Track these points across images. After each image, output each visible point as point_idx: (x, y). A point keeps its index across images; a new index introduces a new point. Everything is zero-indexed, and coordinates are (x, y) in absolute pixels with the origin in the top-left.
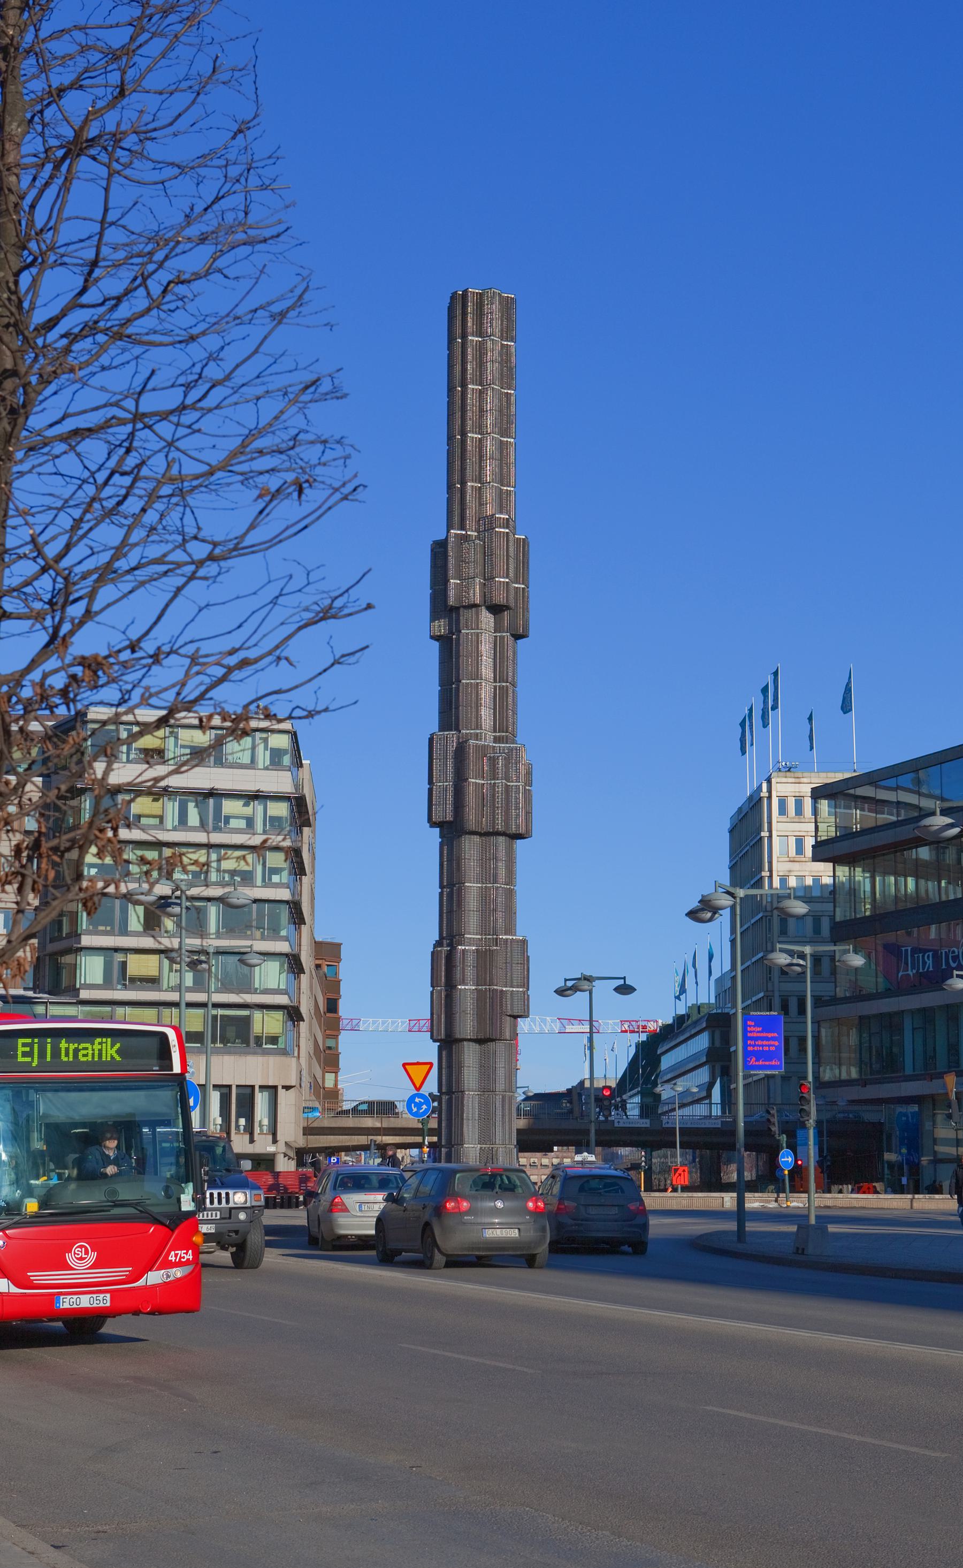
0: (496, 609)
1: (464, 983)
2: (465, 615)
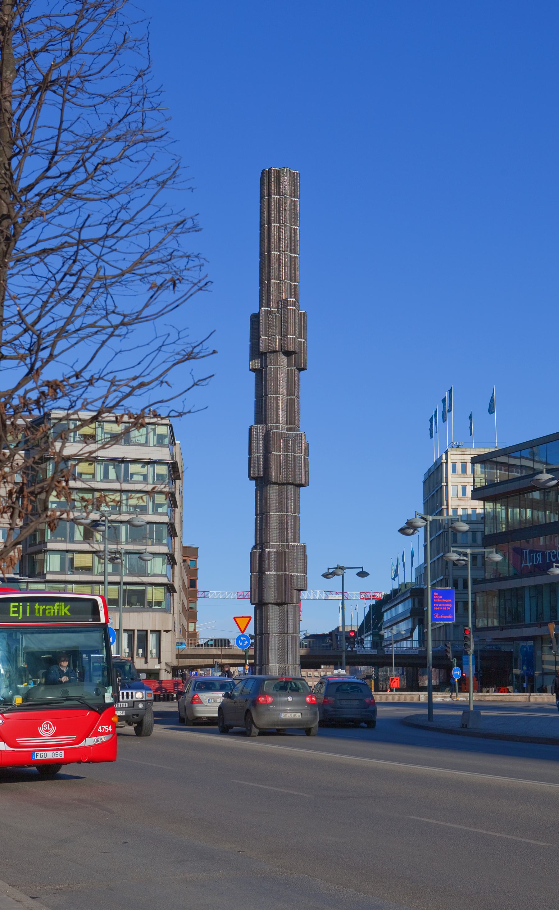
0: (288, 354)
1: (269, 571)
2: (270, 357)
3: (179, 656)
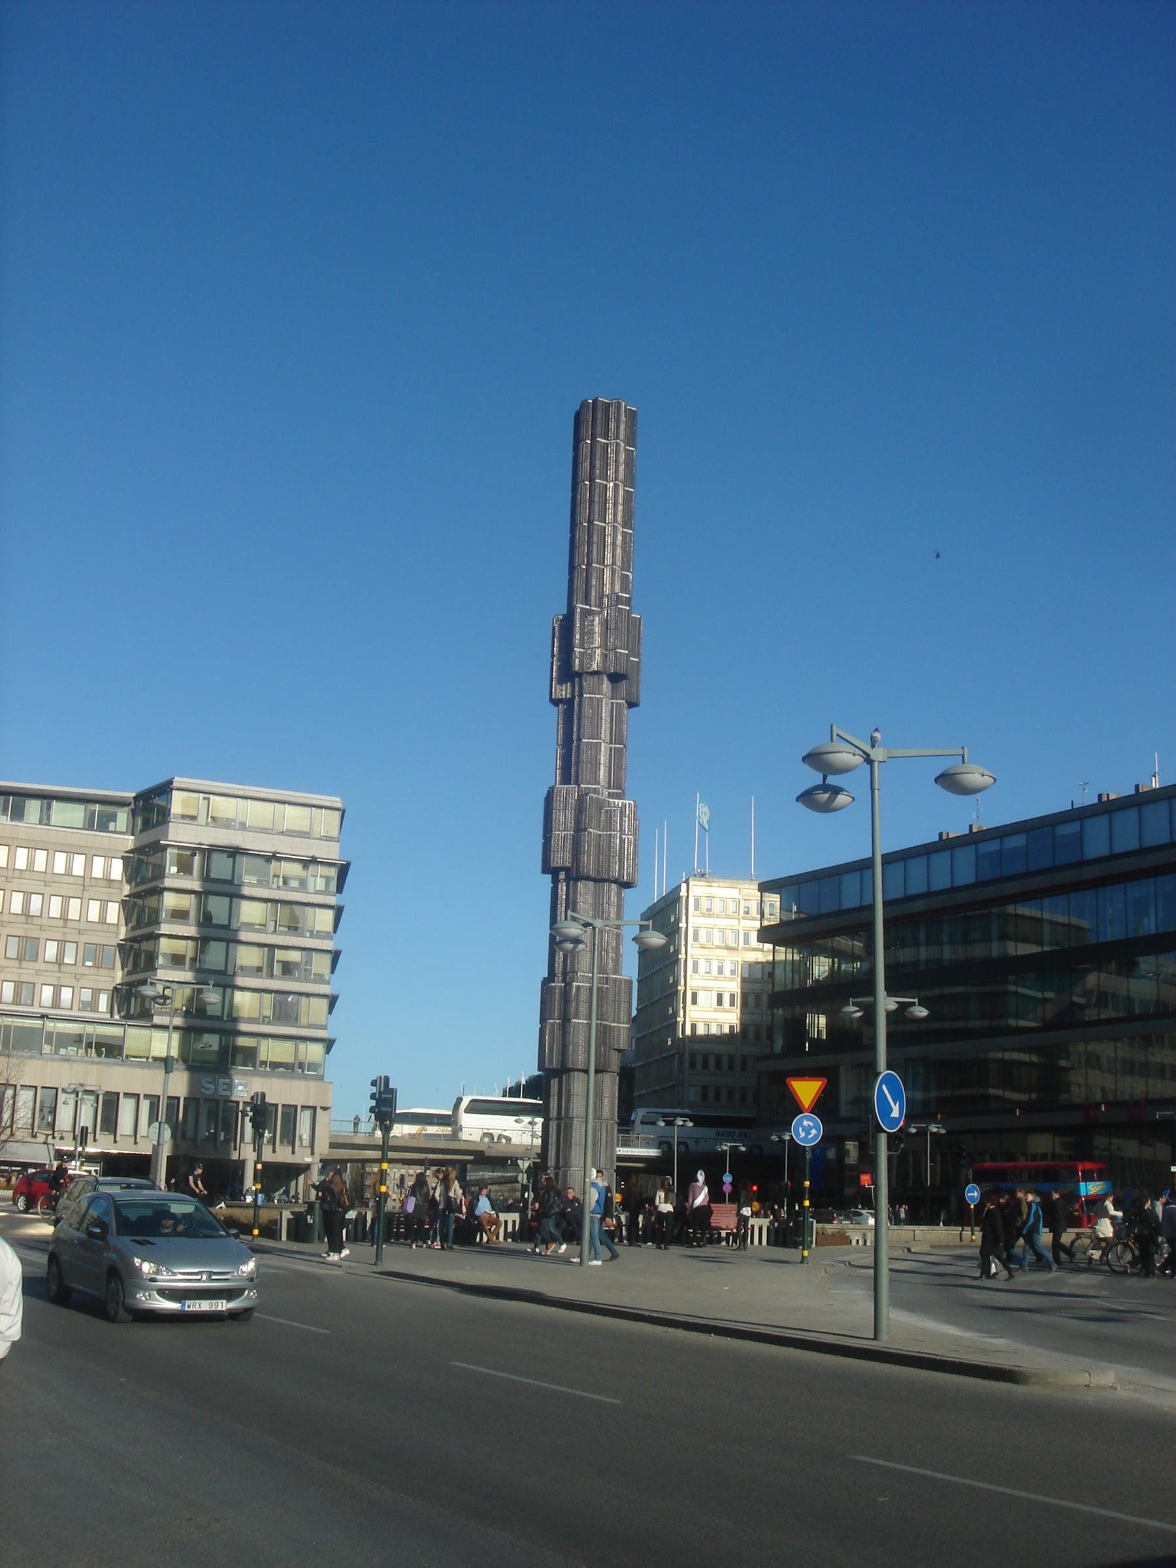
0: (615, 678)
1: (577, 1017)
2: (587, 682)
3: (333, 1145)
